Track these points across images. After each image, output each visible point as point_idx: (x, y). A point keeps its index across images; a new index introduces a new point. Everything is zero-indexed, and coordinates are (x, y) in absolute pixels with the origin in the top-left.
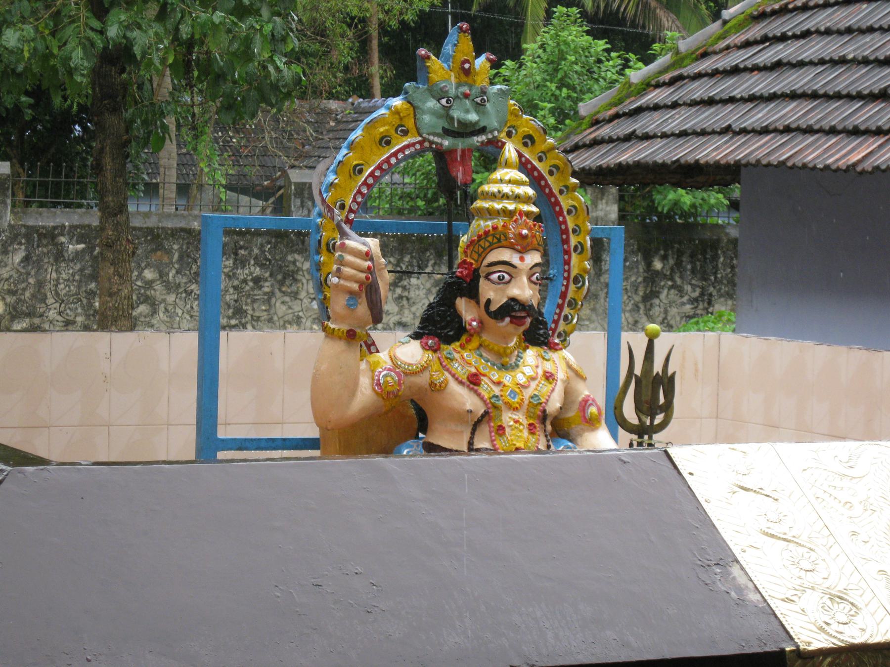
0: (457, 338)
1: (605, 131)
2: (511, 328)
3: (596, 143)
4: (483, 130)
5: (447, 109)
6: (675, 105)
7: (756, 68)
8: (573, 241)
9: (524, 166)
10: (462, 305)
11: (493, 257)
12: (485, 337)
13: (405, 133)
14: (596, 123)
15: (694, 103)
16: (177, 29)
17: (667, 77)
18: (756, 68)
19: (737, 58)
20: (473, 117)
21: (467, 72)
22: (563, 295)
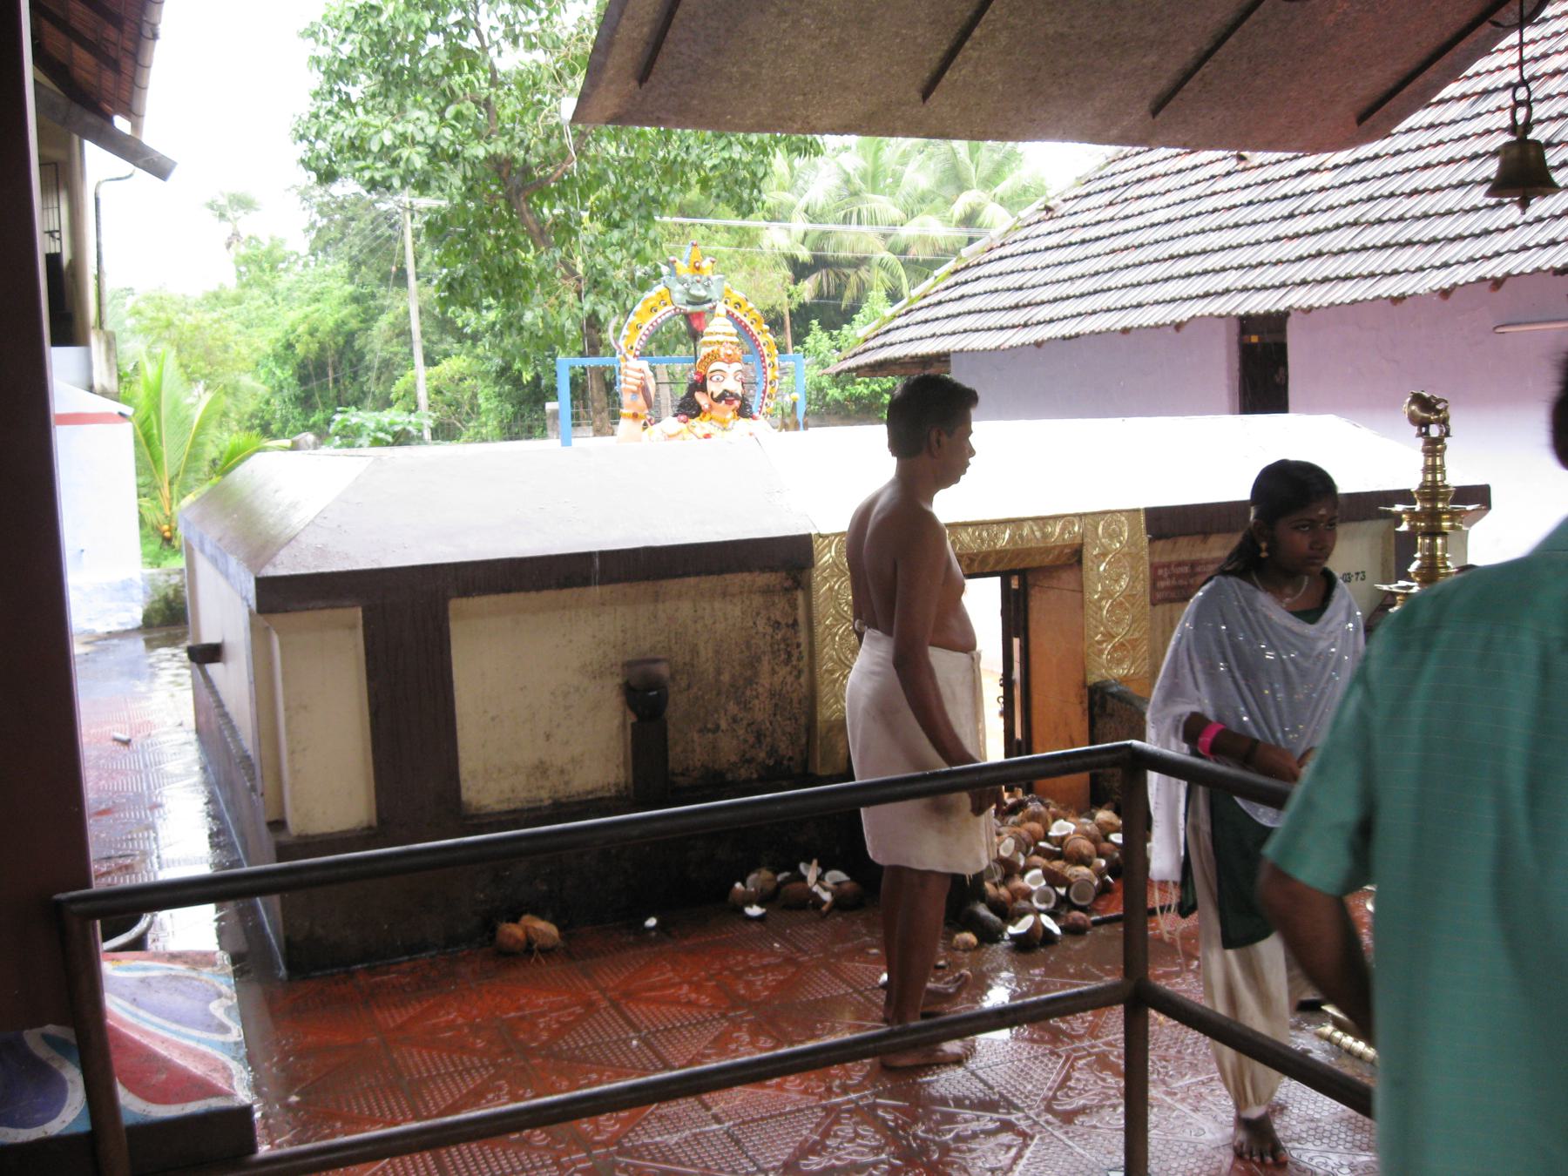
0: (697, 415)
1: (871, 344)
2: (726, 407)
3: (865, 351)
4: (710, 301)
5: (688, 290)
6: (908, 326)
7: (951, 300)
8: (768, 361)
9: (730, 315)
10: (699, 396)
11: (712, 367)
12: (714, 414)
13: (665, 304)
14: (866, 340)
15: (917, 323)
16: (625, 304)
17: (904, 311)
18: (951, 300)
19: (942, 296)
20: (702, 293)
21: (698, 268)
22: (764, 392)
